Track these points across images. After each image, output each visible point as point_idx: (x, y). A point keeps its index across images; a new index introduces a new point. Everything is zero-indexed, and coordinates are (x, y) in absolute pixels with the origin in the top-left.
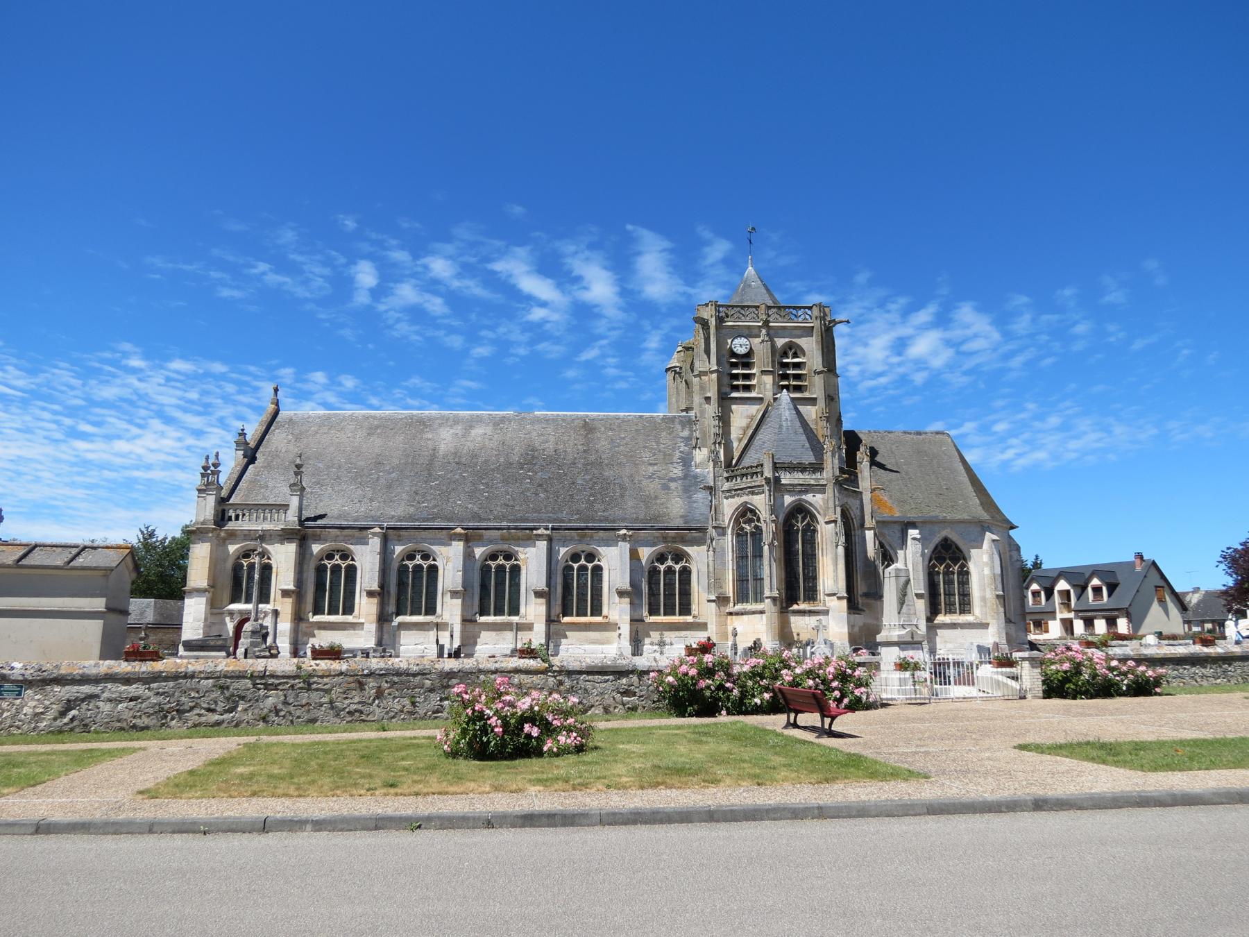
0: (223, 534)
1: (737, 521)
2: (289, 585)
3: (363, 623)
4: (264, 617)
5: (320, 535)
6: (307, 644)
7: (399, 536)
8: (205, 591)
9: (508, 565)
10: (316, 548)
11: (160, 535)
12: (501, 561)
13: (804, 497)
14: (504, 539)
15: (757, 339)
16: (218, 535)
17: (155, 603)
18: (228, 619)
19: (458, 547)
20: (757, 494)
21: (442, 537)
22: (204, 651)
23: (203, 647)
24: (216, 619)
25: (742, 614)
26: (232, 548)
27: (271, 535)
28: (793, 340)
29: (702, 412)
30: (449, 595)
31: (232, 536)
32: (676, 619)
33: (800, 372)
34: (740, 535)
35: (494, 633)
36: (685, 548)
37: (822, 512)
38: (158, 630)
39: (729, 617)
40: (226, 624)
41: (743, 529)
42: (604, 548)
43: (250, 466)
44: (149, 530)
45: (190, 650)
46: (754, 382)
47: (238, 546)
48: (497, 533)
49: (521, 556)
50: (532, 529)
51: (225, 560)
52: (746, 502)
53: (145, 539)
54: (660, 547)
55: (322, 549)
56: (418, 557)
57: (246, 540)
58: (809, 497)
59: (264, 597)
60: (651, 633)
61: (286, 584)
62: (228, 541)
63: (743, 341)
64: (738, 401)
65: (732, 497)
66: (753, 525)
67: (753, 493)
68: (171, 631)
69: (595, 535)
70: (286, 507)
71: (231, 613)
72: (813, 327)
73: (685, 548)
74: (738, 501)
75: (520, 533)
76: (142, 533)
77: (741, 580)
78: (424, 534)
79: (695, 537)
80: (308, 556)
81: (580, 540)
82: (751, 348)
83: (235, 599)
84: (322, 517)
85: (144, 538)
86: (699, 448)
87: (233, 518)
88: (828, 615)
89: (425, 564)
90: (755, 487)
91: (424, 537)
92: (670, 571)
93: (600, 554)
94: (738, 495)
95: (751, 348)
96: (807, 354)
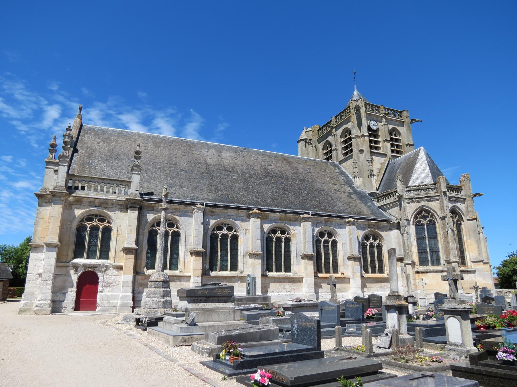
0: (71, 199)
1: (416, 217)
2: (132, 244)
3: (190, 277)
4: (106, 270)
5: (153, 207)
6: (143, 293)
7: (213, 212)
8: (56, 246)
9: (283, 237)
10: (150, 217)
12: (278, 234)
13: (456, 204)
14: (281, 220)
15: (380, 123)
16: (66, 200)
18: (72, 272)
19: (254, 224)
20: (432, 201)
21: (242, 215)
22: (210, 302)
23: (209, 297)
24: (62, 271)
25: (427, 272)
26: (78, 212)
27: (112, 204)
28: (396, 127)
29: (358, 158)
30: (248, 257)
31: (79, 201)
32: (378, 275)
33: (399, 144)
34: (418, 226)
35: (278, 285)
36: (380, 232)
37: (465, 214)
39: (417, 275)
40: (70, 276)
41: (419, 221)
42: (339, 229)
43: (75, 154)
45: (194, 302)
46: (380, 145)
48: (278, 215)
49: (292, 232)
50: (300, 214)
51: (71, 222)
52: (423, 206)
54: (367, 231)
55: (155, 218)
56: (225, 229)
57: (91, 206)
58: (458, 205)
59: (105, 254)
60: (367, 284)
61: (129, 244)
62: (74, 206)
63: (374, 123)
64: (375, 154)
65: (413, 202)
66: (428, 219)
67: (429, 201)
69: (334, 220)
70: (128, 183)
71: (76, 267)
72: (404, 122)
73: (380, 232)
74: (417, 205)
75: (292, 216)
77: (421, 251)
78: (231, 212)
79: (384, 226)
80: (143, 223)
81: (326, 224)
82: (378, 128)
83: (78, 254)
84: (152, 194)
86: (359, 177)
87: (80, 188)
88: (475, 273)
89: (230, 234)
90: (431, 197)
91: (229, 214)
92: (372, 246)
93: (336, 233)
94: (417, 202)
95: (378, 128)
96: (402, 134)
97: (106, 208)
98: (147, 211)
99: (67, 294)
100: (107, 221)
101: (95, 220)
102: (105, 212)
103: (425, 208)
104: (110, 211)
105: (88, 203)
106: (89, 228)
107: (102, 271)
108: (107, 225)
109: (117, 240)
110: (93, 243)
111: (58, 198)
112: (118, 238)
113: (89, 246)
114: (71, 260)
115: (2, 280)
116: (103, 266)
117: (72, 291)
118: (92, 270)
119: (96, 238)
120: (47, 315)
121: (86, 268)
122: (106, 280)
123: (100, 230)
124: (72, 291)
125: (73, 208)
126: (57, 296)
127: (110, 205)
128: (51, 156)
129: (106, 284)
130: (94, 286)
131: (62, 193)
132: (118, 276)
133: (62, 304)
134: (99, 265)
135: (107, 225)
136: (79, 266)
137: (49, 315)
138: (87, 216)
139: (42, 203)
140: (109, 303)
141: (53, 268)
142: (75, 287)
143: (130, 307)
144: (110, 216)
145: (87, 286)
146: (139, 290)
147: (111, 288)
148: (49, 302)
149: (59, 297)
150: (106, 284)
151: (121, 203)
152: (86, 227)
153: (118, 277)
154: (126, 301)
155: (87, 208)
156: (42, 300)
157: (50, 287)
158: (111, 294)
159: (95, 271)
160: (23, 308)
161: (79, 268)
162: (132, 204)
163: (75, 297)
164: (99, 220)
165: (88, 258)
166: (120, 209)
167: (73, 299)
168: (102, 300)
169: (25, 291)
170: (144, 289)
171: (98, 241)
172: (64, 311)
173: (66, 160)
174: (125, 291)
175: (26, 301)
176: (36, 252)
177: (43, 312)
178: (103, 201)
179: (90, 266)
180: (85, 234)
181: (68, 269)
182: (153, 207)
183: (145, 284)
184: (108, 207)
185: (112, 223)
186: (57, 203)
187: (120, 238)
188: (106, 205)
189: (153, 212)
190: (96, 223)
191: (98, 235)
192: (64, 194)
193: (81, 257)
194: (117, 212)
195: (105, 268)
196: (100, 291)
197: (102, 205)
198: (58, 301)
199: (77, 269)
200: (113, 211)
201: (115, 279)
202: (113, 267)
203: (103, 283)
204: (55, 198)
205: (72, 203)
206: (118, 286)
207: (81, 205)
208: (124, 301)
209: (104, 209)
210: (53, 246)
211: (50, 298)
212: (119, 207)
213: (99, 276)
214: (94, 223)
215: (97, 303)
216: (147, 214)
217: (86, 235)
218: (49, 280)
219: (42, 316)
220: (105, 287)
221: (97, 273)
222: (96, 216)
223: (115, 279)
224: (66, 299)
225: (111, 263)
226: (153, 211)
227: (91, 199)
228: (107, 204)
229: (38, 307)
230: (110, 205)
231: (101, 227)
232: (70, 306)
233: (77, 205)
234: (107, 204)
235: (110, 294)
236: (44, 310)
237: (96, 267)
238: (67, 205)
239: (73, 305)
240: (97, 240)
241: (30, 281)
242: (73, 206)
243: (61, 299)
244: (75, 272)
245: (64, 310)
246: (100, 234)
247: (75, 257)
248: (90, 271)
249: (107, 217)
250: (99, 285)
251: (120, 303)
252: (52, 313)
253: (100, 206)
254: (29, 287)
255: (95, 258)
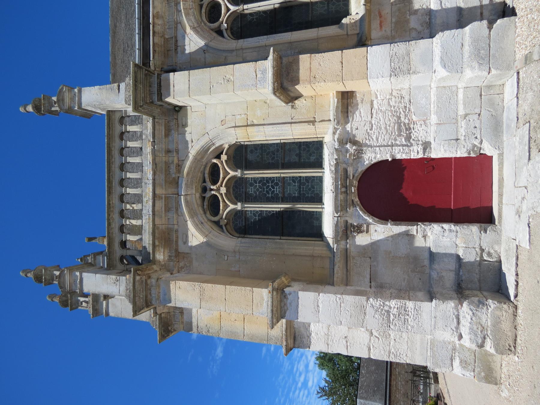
0: (160, 256)
2: (264, 72)
4: (354, 143)
5: (166, 40)
11: (323, 384)
17: (362, 398)
18: (361, 240)
38: (393, 398)
40: (374, 245)
44: (320, 391)
47: (190, 225)
51: (220, 252)
53: (325, 395)
55: (194, 28)
61: (264, 79)
62: (182, 248)
68: (394, 383)
76: (321, 396)
85: (325, 396)
97: (179, 167)
98: (179, 55)
99: (433, 250)
100: (215, 161)
101: (213, 192)
102: (190, 168)
103: (428, 388)
104: (187, 156)
105: (170, 215)
106: (236, 204)
107: (359, 153)
108: (224, 157)
109: (263, 123)
110: (277, 190)
111: (153, 291)
112: (256, 122)
113: (284, 200)
114: (328, 244)
115: (388, 402)
116: (340, 151)
117: (425, 237)
118: (355, 183)
119: (264, 184)
120: (515, 316)
121: (349, 202)
122: (387, 137)
123: (239, 175)
124: (425, 237)
125: (187, 251)
126: (441, 278)
127: (171, 159)
128: (84, 304)
129: (399, 135)
130: (405, 172)
131: (137, 284)
132: (372, 102)
133: (469, 262)
134: (337, 165)
135: (224, 157)
136: (342, 220)
137: (516, 307)
138: (205, 213)
139: (183, 322)
140: (466, 115)
141: (350, 299)
142: (410, 227)
143: (490, 28)
144: (198, 153)
145: (407, 192)
146: (419, 28)
147: (414, 118)
148: (465, 308)
149: (444, 274)
150: (399, 135)
151: (161, 130)
152: (236, 214)
153: (375, 102)
154: (467, 48)
155: (183, 215)
156: (457, 328)
157: (410, 304)
158: (436, 113)
159: (356, 175)
160: (479, 374)
161: (350, 221)
162: (151, 94)
163: (446, 226)
164: (215, 181)
165: (318, 199)
166: (180, 129)
167: (450, 231)
168: (457, 139)
169: (424, 364)
170: (417, 11)
171: (270, 178)
172: (494, 255)
173: (67, 277)
174: (428, 60)
175: (456, 363)
176: (309, 337)
177: (506, 326)
178: (161, 177)
179: (343, 190)
180: (255, 213)
181: (353, 252)
182: (166, 40)
183: (399, 10)
184: (176, 161)
185: (217, 145)
186: (165, 295)
187: (256, 117)
188: (173, 169)
189: (179, 38)
190: (222, 189)
191: (255, 180)
192: (138, 278)
193: (318, 217)
194: (188, 137)
195: (348, 146)
196: (425, 150)
197: (174, 178)
198: (457, 273)
199: (354, 227)
200: (187, 148)
201: (384, 109)
202: (342, 121)
203: (397, 145)
204: (154, 299)
205: (174, 254)
206: (407, 100)
207: (177, 231)
208: (466, 55)
209: (181, 171)
210: (281, 301)
211: (451, 304)
212: (174, 134)
213: (374, 161)
214: (221, 194)
215: (466, 155)
216: (187, 52)
217: (257, 212)
218: (386, 308)
219: (519, 333)
220: (408, 138)
221: (364, 168)
222: (205, 190)
223: (384, 109)
224: (453, 252)
225: (331, 131)
226: (176, 37)
227: (157, 208)
228: (167, 165)
229: (483, 342)
230: (171, 159)
231: (232, 173)
232: (477, 240)
233: (177, 242)
234: (167, 165)
235: (434, 119)
236: (497, 323)
237: (346, 171)
238: (181, 264)
239: (474, 228)
240: (268, 180)
241: (393, 350)
242: (180, 250)
243: (452, 265)
244: (361, 232)
245: (489, 254)
246: (251, 174)
247: (319, 235)
248: (359, 189)
249: (204, 160)
250: (404, 157)
251: (472, 68)
252: (508, 297)
253: (176, 183)
254: (409, 354)
255: (320, 180)
